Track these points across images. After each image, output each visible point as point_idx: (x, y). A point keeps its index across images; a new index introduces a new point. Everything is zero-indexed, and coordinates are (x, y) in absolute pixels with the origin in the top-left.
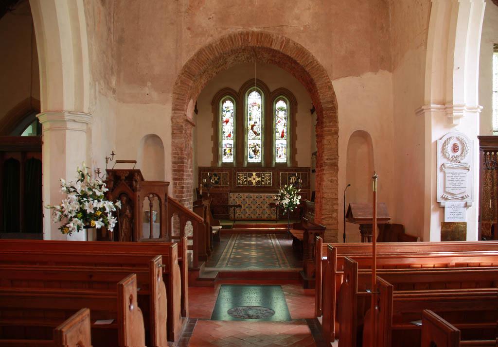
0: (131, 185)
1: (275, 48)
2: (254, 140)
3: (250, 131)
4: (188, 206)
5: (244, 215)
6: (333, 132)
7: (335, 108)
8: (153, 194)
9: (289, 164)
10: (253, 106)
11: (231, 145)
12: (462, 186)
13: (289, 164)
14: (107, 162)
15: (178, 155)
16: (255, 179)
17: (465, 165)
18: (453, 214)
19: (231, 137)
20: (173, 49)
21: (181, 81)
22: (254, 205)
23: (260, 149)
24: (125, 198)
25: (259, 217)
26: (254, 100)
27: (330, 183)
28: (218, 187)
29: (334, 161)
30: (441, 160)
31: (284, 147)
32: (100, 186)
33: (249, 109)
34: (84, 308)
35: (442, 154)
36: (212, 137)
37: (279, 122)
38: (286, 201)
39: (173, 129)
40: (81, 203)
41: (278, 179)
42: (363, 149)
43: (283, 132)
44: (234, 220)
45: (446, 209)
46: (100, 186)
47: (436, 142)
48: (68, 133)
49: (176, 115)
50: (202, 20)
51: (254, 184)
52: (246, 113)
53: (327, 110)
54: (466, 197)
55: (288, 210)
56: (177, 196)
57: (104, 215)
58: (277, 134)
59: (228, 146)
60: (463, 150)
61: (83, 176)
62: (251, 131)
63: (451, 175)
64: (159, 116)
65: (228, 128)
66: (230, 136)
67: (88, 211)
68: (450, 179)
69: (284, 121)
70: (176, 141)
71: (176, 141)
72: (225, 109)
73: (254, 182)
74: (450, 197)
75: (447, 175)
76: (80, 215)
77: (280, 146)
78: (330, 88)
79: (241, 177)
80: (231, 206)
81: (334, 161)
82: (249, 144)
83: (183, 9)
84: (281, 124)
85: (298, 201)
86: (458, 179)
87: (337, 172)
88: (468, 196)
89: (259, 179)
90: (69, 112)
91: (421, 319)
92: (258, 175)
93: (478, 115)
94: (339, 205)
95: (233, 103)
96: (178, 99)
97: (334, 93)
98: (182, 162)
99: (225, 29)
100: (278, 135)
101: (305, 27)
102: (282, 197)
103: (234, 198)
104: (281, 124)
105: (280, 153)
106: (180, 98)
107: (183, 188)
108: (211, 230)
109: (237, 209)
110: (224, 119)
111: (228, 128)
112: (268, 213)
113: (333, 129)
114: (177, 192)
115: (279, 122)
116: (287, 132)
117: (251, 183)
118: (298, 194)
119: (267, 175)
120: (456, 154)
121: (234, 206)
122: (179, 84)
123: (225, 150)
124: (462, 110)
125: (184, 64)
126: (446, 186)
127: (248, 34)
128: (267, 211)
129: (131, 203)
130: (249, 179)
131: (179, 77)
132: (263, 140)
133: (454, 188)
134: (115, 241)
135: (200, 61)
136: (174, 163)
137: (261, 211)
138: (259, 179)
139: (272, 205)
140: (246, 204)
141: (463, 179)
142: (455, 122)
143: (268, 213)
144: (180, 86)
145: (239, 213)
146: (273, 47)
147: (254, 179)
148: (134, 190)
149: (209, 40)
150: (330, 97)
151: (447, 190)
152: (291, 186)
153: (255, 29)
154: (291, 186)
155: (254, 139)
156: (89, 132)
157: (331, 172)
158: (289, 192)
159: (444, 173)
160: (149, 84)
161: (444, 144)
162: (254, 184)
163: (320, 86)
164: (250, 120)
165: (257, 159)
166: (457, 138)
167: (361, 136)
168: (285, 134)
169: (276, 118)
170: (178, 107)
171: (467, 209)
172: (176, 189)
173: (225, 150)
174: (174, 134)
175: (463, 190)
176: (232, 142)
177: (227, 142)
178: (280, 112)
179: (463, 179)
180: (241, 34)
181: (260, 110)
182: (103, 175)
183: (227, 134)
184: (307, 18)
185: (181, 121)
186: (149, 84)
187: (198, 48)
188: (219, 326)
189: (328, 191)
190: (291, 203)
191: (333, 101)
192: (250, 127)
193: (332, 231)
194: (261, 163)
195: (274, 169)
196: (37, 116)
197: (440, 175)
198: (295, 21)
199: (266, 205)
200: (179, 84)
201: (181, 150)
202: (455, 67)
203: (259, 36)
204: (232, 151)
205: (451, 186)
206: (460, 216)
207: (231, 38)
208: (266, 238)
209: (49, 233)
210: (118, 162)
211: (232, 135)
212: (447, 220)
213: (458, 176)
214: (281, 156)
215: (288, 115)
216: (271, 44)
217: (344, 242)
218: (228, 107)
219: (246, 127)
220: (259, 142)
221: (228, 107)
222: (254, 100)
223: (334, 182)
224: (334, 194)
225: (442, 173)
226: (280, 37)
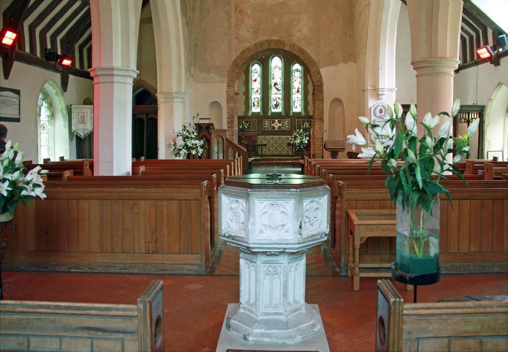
0: (208, 131)
1: (287, 50)
2: (276, 96)
3: (273, 88)
4: (236, 142)
5: (269, 152)
8: (219, 136)
9: (303, 114)
10: (275, 68)
11: (259, 98)
13: (303, 114)
14: (194, 119)
16: (277, 125)
19: (259, 93)
20: (225, 53)
21: (232, 70)
22: (280, 148)
23: (281, 101)
24: (205, 139)
25: (280, 153)
26: (276, 63)
28: (249, 131)
31: (299, 99)
32: (193, 133)
33: (272, 70)
36: (244, 93)
37: (295, 80)
38: (298, 141)
40: (185, 141)
41: (295, 124)
42: (339, 109)
43: (299, 88)
44: (262, 156)
46: (193, 133)
48: (175, 104)
50: (244, 33)
51: (276, 129)
52: (270, 73)
55: (299, 147)
57: (197, 148)
58: (294, 90)
59: (256, 99)
60: (385, 112)
61: (185, 127)
62: (274, 88)
64: (219, 91)
65: (256, 86)
66: (257, 91)
67: (189, 146)
69: (299, 80)
70: (230, 105)
71: (230, 105)
72: (254, 71)
73: (276, 127)
76: (185, 147)
77: (296, 99)
78: (319, 73)
79: (266, 123)
80: (259, 145)
82: (272, 97)
83: (233, 26)
84: (297, 82)
85: (306, 141)
87: (323, 123)
89: (280, 125)
90: (176, 93)
91: (440, 253)
92: (279, 122)
93: (395, 93)
95: (260, 66)
98: (233, 118)
99: (257, 38)
100: (294, 91)
101: (304, 36)
102: (295, 138)
103: (261, 139)
104: (297, 82)
105: (296, 104)
107: (233, 132)
108: (248, 160)
109: (264, 148)
110: (253, 79)
111: (256, 86)
112: (287, 150)
115: (295, 80)
116: (301, 88)
117: (274, 128)
118: (306, 136)
119: (286, 121)
120: (381, 115)
121: (262, 145)
123: (254, 102)
127: (271, 41)
128: (286, 148)
129: (208, 141)
130: (272, 125)
132: (283, 94)
136: (228, 118)
137: (281, 149)
138: (280, 125)
139: (289, 144)
140: (271, 144)
142: (380, 97)
143: (287, 150)
145: (265, 151)
146: (285, 49)
147: (276, 125)
148: (210, 134)
149: (248, 45)
152: (302, 130)
153: (275, 38)
154: (302, 130)
155: (276, 94)
156: (184, 102)
158: (300, 135)
160: (213, 71)
162: (276, 129)
164: (273, 79)
165: (279, 110)
167: (337, 101)
168: (300, 90)
169: (293, 77)
170: (230, 85)
173: (254, 102)
176: (259, 96)
177: (256, 96)
178: (296, 72)
180: (266, 41)
181: (281, 71)
182: (193, 125)
183: (255, 90)
184: (305, 31)
185: (232, 93)
186: (213, 71)
187: (242, 49)
190: (301, 142)
192: (273, 84)
194: (281, 112)
195: (291, 117)
198: (298, 33)
199: (286, 144)
201: (232, 110)
202: (380, 68)
203: (278, 42)
204: (260, 103)
207: (261, 44)
208: (285, 167)
209: (162, 155)
210: (200, 119)
211: (259, 91)
212: (92, 106)
214: (297, 107)
215: (303, 75)
216: (284, 47)
217: (478, 158)
218: (256, 69)
219: (270, 85)
220: (280, 96)
221: (256, 69)
222: (276, 63)
223: (321, 128)
226: (290, 42)
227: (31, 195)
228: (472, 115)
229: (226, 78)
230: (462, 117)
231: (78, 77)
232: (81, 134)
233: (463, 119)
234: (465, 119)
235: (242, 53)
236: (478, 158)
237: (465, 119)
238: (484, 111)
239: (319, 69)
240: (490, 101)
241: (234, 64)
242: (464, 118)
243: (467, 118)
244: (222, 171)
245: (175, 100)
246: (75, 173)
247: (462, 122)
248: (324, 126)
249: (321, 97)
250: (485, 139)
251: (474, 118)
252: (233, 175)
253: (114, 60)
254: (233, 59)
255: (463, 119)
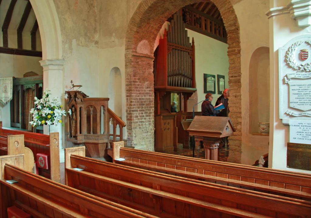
6: (236, 51)
7: (237, 29)
15: (129, 79)
18: (302, 134)
27: (234, 98)
29: (238, 78)
30: (283, 71)
35: (285, 64)
39: (126, 62)
45: (291, 128)
47: (277, 51)
49: (127, 53)
53: (230, 33)
56: (128, 107)
68: (296, 92)
70: (128, 70)
74: (296, 113)
75: (291, 88)
78: (233, 11)
81: (238, 78)
94: (242, 118)
96: (129, 41)
97: (236, 17)
106: (130, 40)
114: (128, 105)
120: (303, 63)
122: (129, 31)
125: (131, 16)
126: (291, 101)
131: (129, 26)
133: (303, 104)
134: (36, 133)
135: (140, 12)
136: (127, 85)
144: (130, 33)
150: (232, 20)
151: (291, 105)
157: (235, 88)
161: (287, 52)
163: (224, 12)
166: (306, 42)
170: (129, 47)
172: (127, 103)
174: (127, 65)
186: (114, 34)
191: (235, 23)
193: (237, 141)
196: (40, 61)
197: (283, 89)
200: (129, 31)
205: (297, 100)
212: (292, 141)
213: (307, 88)
224: (238, 109)
225: (286, 86)
227: (100, 152)
229: (125, 39)
231: (15, 56)
232: (4, 101)
235: (139, 7)
239: (232, 7)
241: (133, 22)
244: (304, 155)
245: (51, 67)
248: (242, 93)
249: (236, 49)
254: (131, 17)
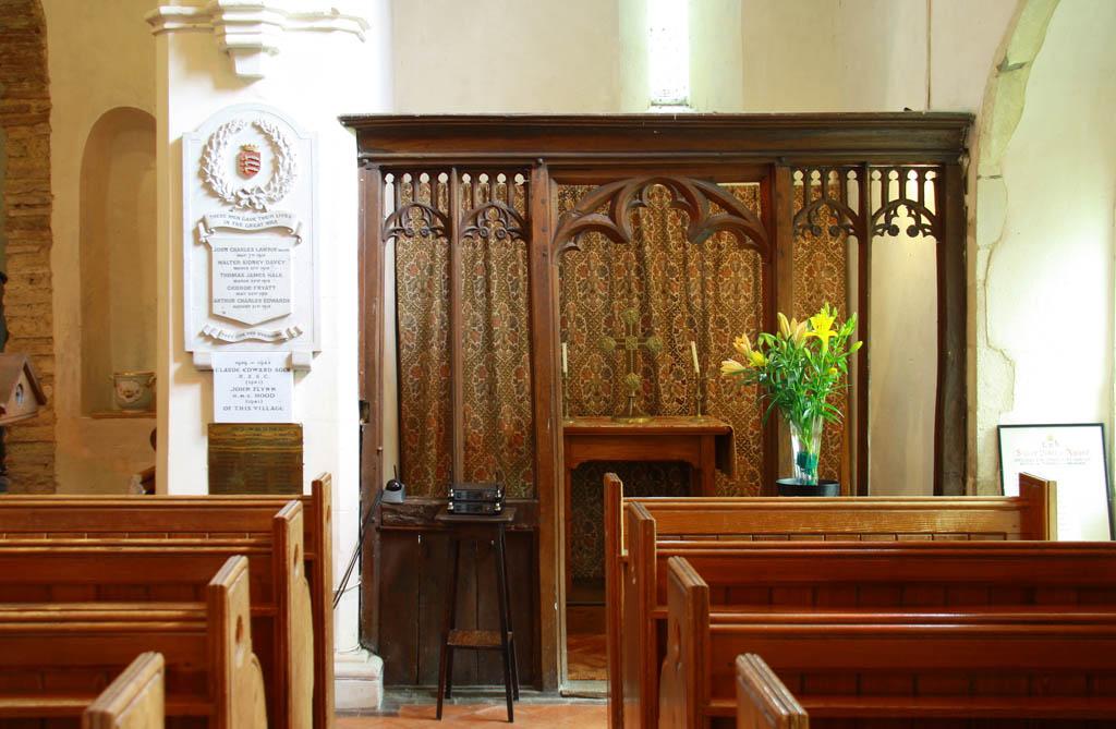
7: (38, 31)
12: (272, 294)
17: (282, 222)
29: (40, 211)
30: (196, 205)
34: (147, 650)
54: (292, 337)
63: (231, 256)
68: (229, 269)
74: (229, 332)
75: (217, 256)
81: (40, 211)
86: (259, 271)
88: (300, 333)
94: (57, 358)
113: (33, 104)
120: (249, 184)
124: (257, 23)
126: (215, 297)
133: (246, 304)
141: (277, 269)
151: (217, 309)
157: (29, 248)
159: (207, 245)
166: (255, 126)
171: (296, 380)
175: (276, 310)
179: (277, 269)
188: (128, 719)
189: (23, 313)
197: (194, 258)
205: (232, 294)
206: (268, 402)
213: (255, 259)
217: (938, 491)
224: (41, 324)
228: (885, 181)
230: (894, 195)
233: (902, 210)
234: (917, 208)
236: (938, 491)
237: (917, 208)
238: (966, 152)
240: (1003, 77)
242: (910, 205)
243: (854, 203)
246: (481, 508)
247: (894, 231)
249: (33, 104)
250: (981, 342)
251: (903, 199)
252: (271, 549)
253: (777, 177)
255: (902, 210)
